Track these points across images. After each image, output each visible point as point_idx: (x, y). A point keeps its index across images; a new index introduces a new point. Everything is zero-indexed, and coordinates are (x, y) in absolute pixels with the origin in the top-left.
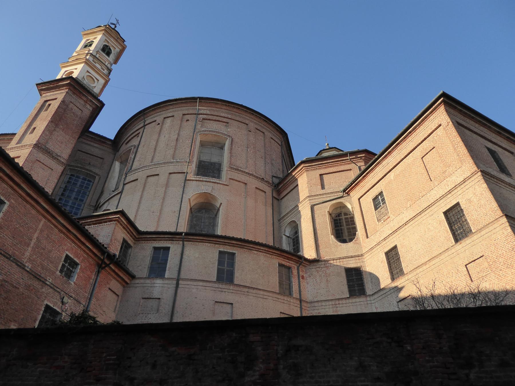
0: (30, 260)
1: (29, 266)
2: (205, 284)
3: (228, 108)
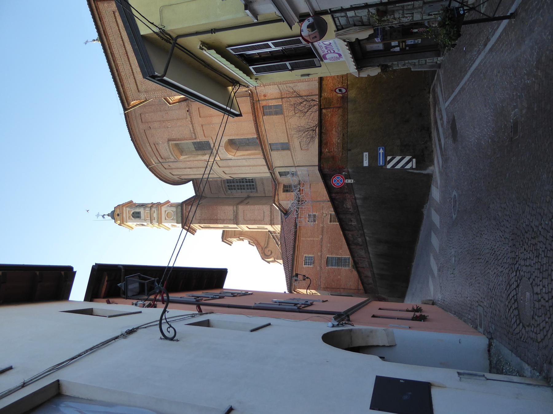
0: (318, 237)
1: (320, 236)
2: (293, 156)
3: (141, 147)
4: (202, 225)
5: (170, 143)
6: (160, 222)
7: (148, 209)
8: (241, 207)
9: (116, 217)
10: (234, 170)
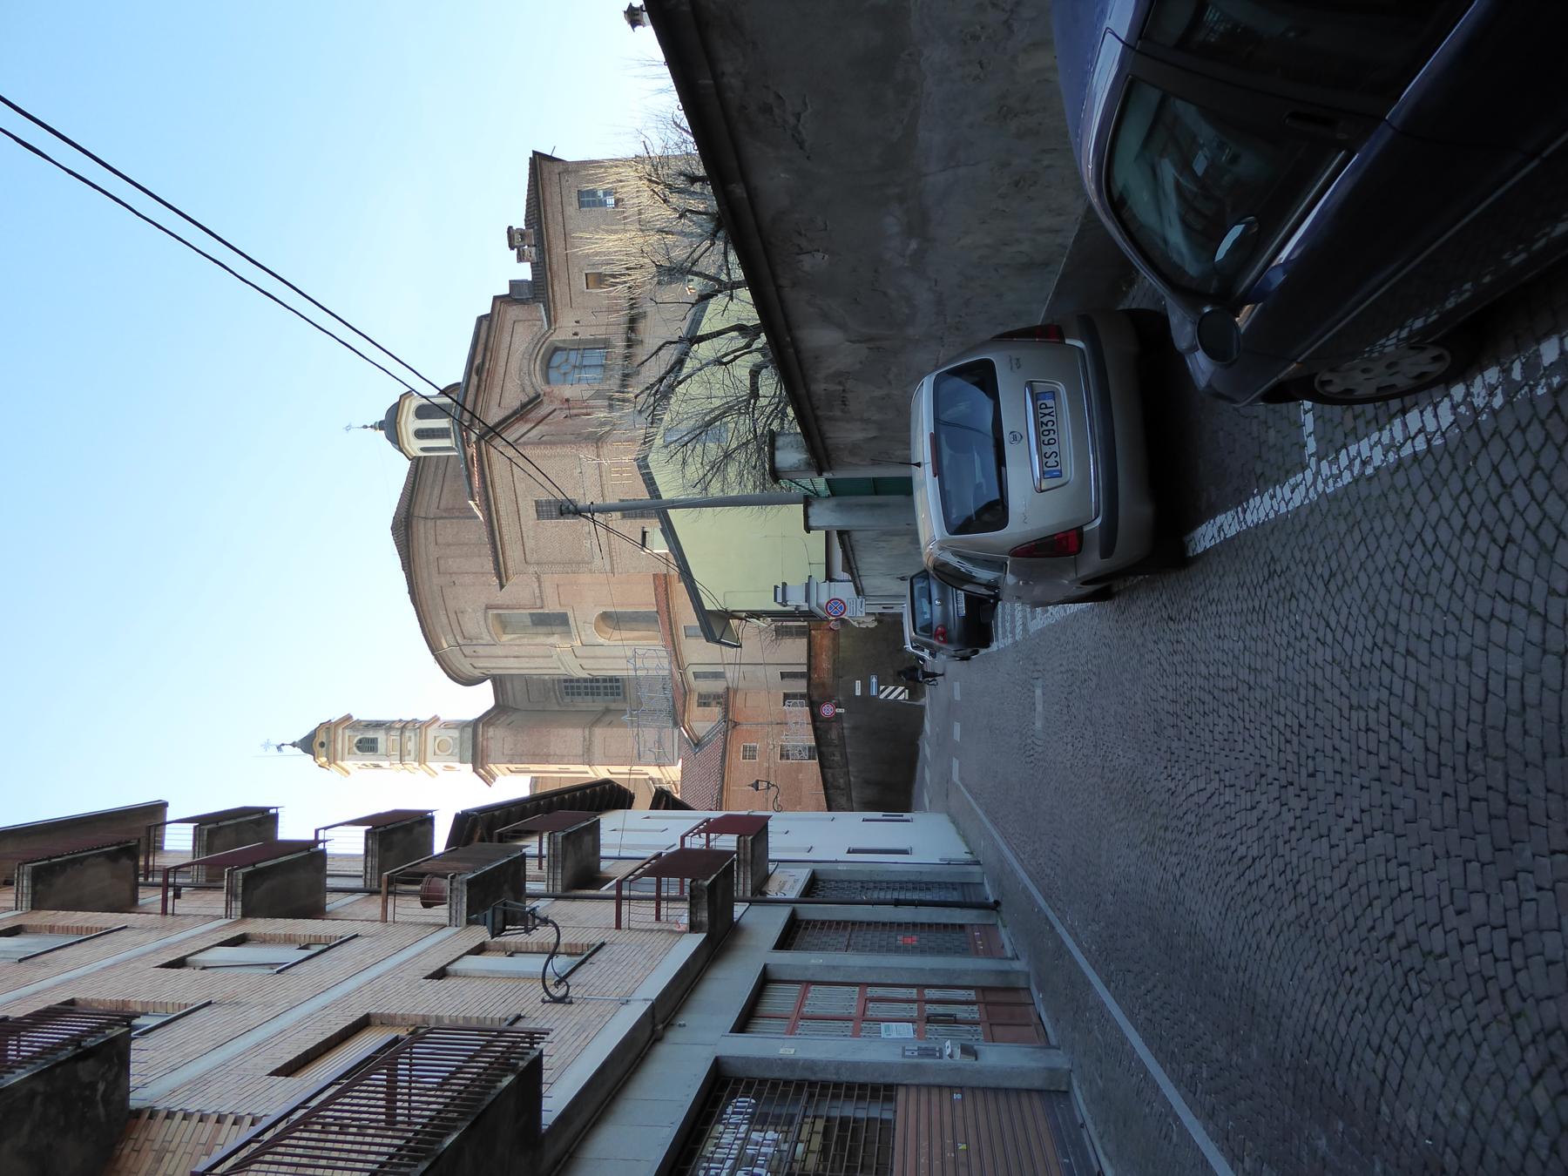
4: (512, 767)
5: (490, 612)
6: (421, 759)
7: (395, 735)
8: (599, 732)
9: (316, 747)
10: (602, 664)
